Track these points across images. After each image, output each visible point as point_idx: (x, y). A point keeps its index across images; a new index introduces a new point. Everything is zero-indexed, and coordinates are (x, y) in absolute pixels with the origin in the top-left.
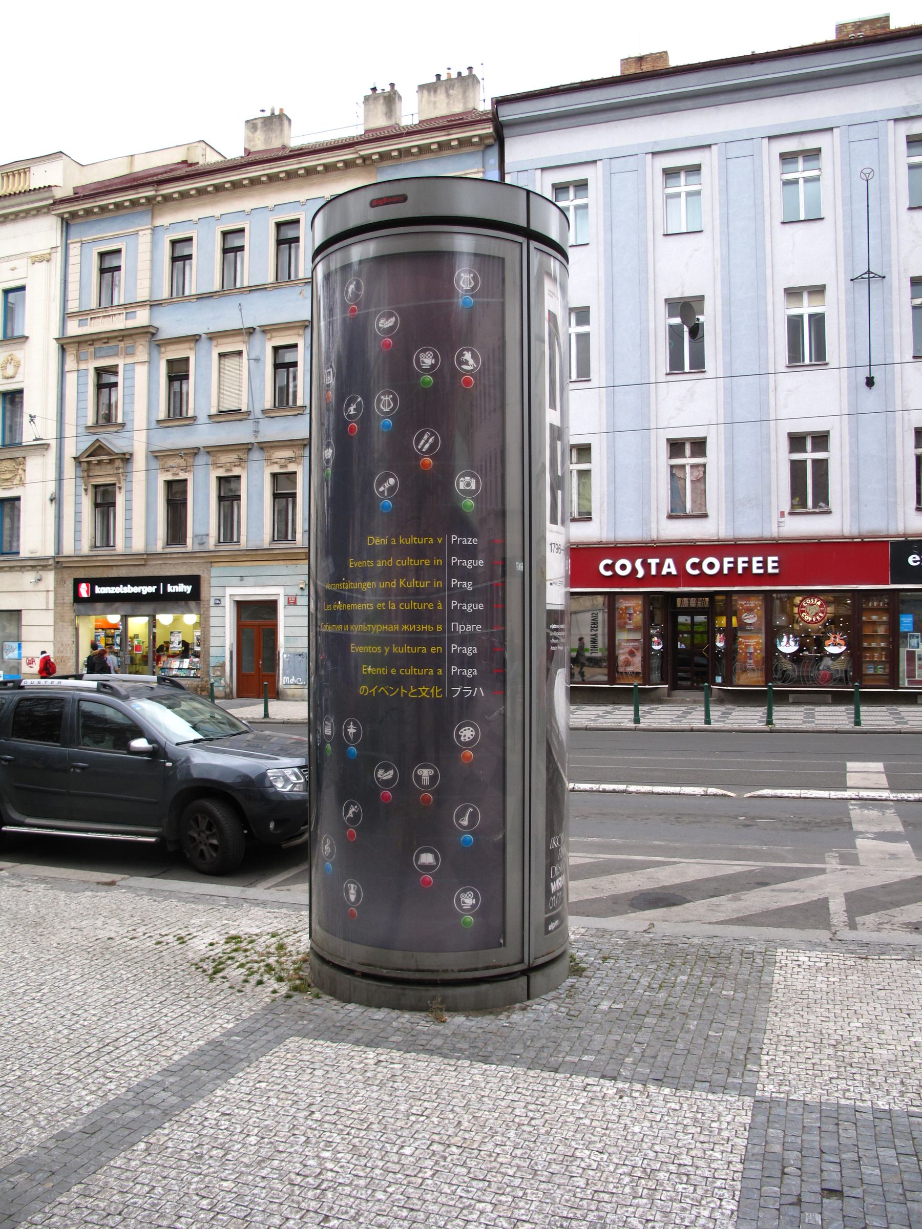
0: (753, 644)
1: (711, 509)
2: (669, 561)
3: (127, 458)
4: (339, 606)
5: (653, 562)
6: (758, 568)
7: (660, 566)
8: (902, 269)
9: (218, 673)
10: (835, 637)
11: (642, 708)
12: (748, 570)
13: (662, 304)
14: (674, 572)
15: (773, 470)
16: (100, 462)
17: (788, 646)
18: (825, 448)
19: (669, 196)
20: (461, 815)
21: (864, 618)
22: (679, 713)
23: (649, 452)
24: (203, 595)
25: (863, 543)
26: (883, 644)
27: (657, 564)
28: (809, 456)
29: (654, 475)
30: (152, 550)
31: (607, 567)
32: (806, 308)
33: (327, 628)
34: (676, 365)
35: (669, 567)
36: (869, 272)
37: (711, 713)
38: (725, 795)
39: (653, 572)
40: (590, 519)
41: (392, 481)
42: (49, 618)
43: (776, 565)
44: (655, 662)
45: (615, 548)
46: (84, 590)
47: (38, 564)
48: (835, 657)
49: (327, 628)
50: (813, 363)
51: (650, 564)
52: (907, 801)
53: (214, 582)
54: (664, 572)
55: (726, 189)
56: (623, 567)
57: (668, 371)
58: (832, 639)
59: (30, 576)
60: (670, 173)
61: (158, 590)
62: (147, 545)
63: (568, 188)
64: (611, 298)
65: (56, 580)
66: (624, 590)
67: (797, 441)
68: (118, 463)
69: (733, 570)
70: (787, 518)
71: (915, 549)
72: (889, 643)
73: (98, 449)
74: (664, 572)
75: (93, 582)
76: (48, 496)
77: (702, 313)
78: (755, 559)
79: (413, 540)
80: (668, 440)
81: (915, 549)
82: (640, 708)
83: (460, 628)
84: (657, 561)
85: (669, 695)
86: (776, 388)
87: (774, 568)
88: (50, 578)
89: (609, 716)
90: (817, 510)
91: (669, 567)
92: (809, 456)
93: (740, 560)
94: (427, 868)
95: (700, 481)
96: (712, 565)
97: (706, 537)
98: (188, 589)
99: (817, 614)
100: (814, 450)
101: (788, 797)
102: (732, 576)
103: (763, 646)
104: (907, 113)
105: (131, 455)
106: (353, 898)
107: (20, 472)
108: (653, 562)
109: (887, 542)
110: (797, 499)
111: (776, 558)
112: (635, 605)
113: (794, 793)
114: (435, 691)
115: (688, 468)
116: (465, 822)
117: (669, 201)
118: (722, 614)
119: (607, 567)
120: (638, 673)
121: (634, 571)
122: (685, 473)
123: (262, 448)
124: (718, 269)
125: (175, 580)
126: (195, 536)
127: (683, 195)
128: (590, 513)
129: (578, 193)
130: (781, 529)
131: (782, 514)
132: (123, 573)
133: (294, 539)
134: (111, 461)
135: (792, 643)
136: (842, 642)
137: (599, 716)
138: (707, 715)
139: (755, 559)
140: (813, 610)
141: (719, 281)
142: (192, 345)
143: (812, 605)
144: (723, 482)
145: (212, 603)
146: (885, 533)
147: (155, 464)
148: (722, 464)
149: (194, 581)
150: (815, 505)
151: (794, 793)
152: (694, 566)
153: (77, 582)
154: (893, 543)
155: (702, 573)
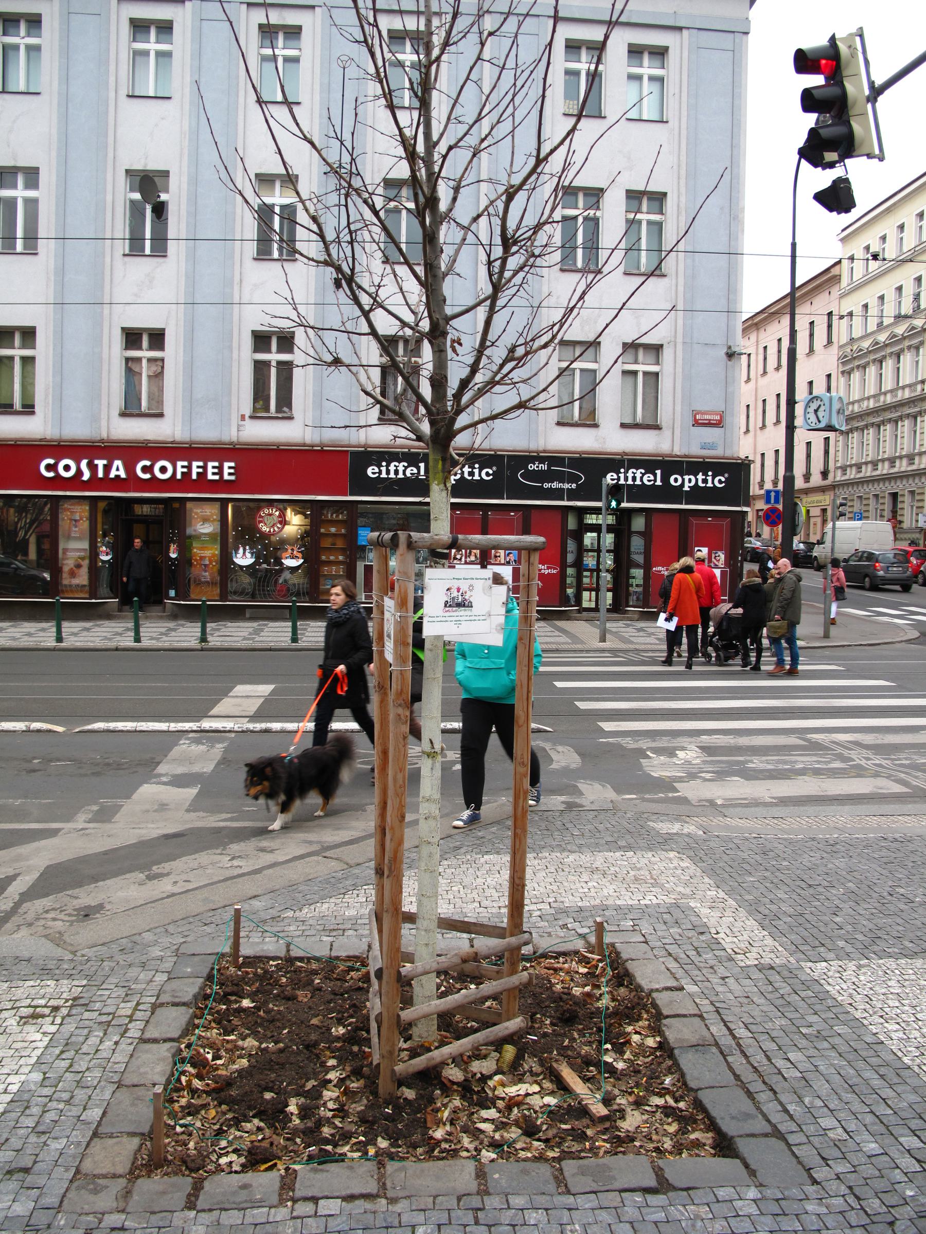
0: (208, 553)
1: (168, 409)
2: (118, 463)
5: (101, 463)
6: (214, 474)
7: (107, 468)
8: (376, 169)
10: (293, 550)
11: (210, 626)
12: (202, 475)
13: (123, 174)
15: (235, 369)
17: (244, 558)
18: (33, 347)
19: (137, 54)
21: (322, 530)
22: (163, 630)
23: (102, 341)
25: (322, 451)
26: (341, 558)
27: (105, 466)
28: (274, 357)
29: (105, 367)
31: (49, 468)
32: (278, 198)
34: (136, 247)
35: (118, 469)
37: (63, 630)
38: (50, 731)
39: (101, 474)
40: (33, 413)
43: (232, 471)
44: (105, 576)
45: (59, 446)
48: (294, 570)
50: (284, 257)
51: (97, 466)
52: (252, 731)
54: (112, 475)
55: (198, 54)
56: (67, 468)
57: (127, 252)
58: (290, 551)
63: (18, 21)
64: (64, 161)
66: (68, 493)
67: (261, 340)
70: (248, 422)
71: (374, 460)
72: (347, 557)
74: (112, 475)
77: (167, 191)
80: (123, 329)
81: (374, 460)
82: (208, 625)
84: (105, 462)
85: (120, 610)
86: (241, 280)
87: (230, 474)
89: (173, 634)
90: (280, 416)
95: (158, 377)
96: (164, 469)
97: (160, 438)
99: (273, 526)
100: (279, 351)
101: (122, 731)
102: (186, 482)
103: (217, 558)
104: (389, 5)
108: (101, 463)
109: (347, 451)
110: (261, 402)
111: (233, 464)
112: (81, 512)
113: (129, 725)
115: (144, 362)
117: (138, 58)
119: (49, 468)
120: (84, 586)
121: (79, 472)
122: (141, 367)
124: (186, 143)
128: (33, 406)
129: (32, 31)
130: (241, 433)
131: (243, 418)
135: (248, 555)
136: (300, 555)
137: (162, 634)
138: (59, 632)
141: (186, 158)
143: (270, 515)
144: (181, 379)
146: (346, 443)
148: (181, 359)
150: (279, 410)
151: (129, 725)
152: (145, 469)
154: (353, 453)
155: (154, 477)
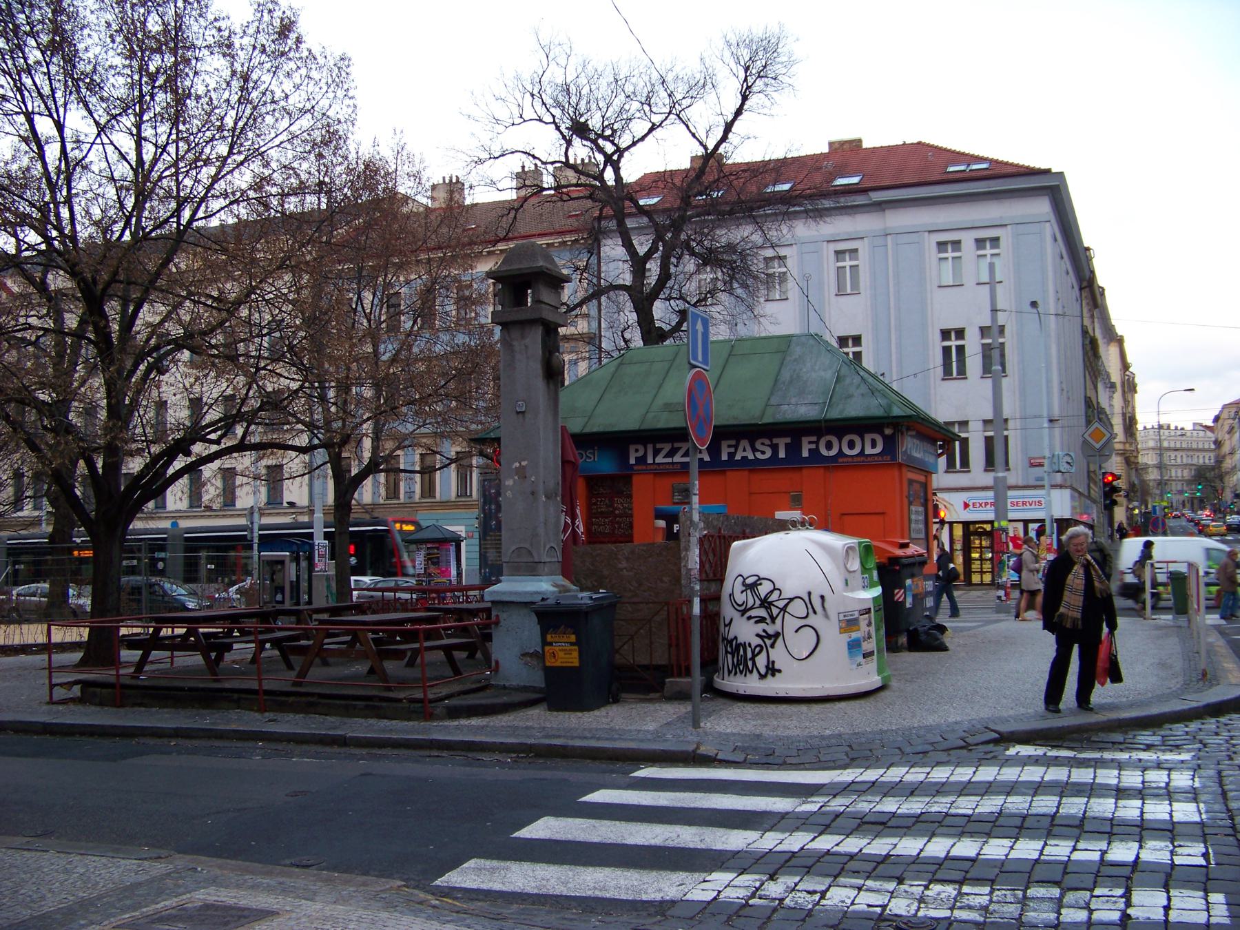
28: (953, 343)
60: (942, 246)
92: (953, 343)
127: (950, 259)
133: (471, 495)
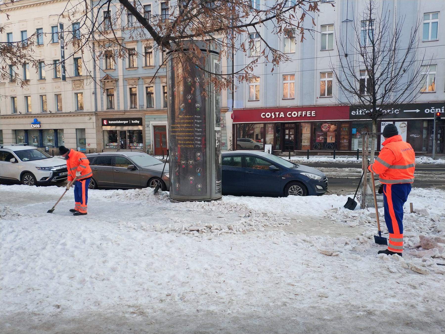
3: (117, 81)
4: (173, 130)
5: (277, 113)
7: (279, 115)
9: (149, 148)
14: (283, 116)
16: (108, 82)
20: (198, 170)
24: (143, 124)
30: (126, 110)
31: (263, 115)
33: (171, 134)
35: (282, 115)
36: (347, 19)
41: (183, 105)
42: (94, 131)
43: (314, 114)
46: (105, 122)
47: (90, 114)
49: (171, 134)
53: (146, 120)
56: (268, 115)
59: (87, 118)
61: (129, 122)
62: (124, 108)
65: (96, 119)
66: (268, 122)
68: (114, 82)
69: (301, 115)
73: (107, 77)
75: (108, 120)
76: (92, 92)
78: (308, 112)
79: (188, 117)
83: (197, 134)
84: (278, 113)
88: (94, 118)
91: (282, 115)
93: (304, 112)
94: (191, 180)
96: (295, 114)
98: (138, 122)
105: (118, 79)
106: (177, 186)
107: (82, 84)
108: (277, 113)
111: (314, 112)
114: (192, 146)
116: (199, 171)
118: (287, 129)
119: (263, 115)
123: (159, 78)
125: (134, 119)
126: (140, 105)
132: (117, 117)
134: (112, 81)
139: (308, 112)
140: (326, 127)
142: (136, 43)
143: (325, 126)
145: (146, 126)
147: (126, 83)
149: (140, 119)
153: (103, 120)
155: (292, 116)
